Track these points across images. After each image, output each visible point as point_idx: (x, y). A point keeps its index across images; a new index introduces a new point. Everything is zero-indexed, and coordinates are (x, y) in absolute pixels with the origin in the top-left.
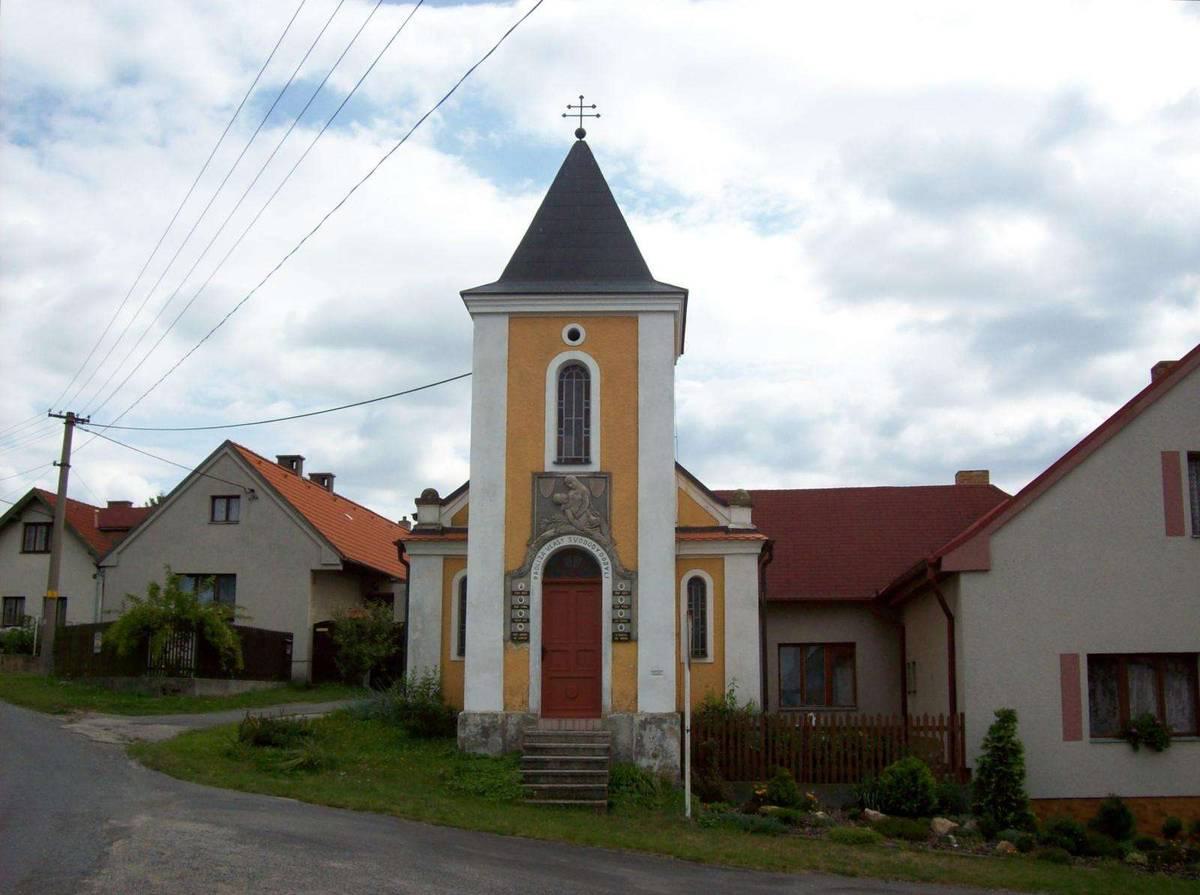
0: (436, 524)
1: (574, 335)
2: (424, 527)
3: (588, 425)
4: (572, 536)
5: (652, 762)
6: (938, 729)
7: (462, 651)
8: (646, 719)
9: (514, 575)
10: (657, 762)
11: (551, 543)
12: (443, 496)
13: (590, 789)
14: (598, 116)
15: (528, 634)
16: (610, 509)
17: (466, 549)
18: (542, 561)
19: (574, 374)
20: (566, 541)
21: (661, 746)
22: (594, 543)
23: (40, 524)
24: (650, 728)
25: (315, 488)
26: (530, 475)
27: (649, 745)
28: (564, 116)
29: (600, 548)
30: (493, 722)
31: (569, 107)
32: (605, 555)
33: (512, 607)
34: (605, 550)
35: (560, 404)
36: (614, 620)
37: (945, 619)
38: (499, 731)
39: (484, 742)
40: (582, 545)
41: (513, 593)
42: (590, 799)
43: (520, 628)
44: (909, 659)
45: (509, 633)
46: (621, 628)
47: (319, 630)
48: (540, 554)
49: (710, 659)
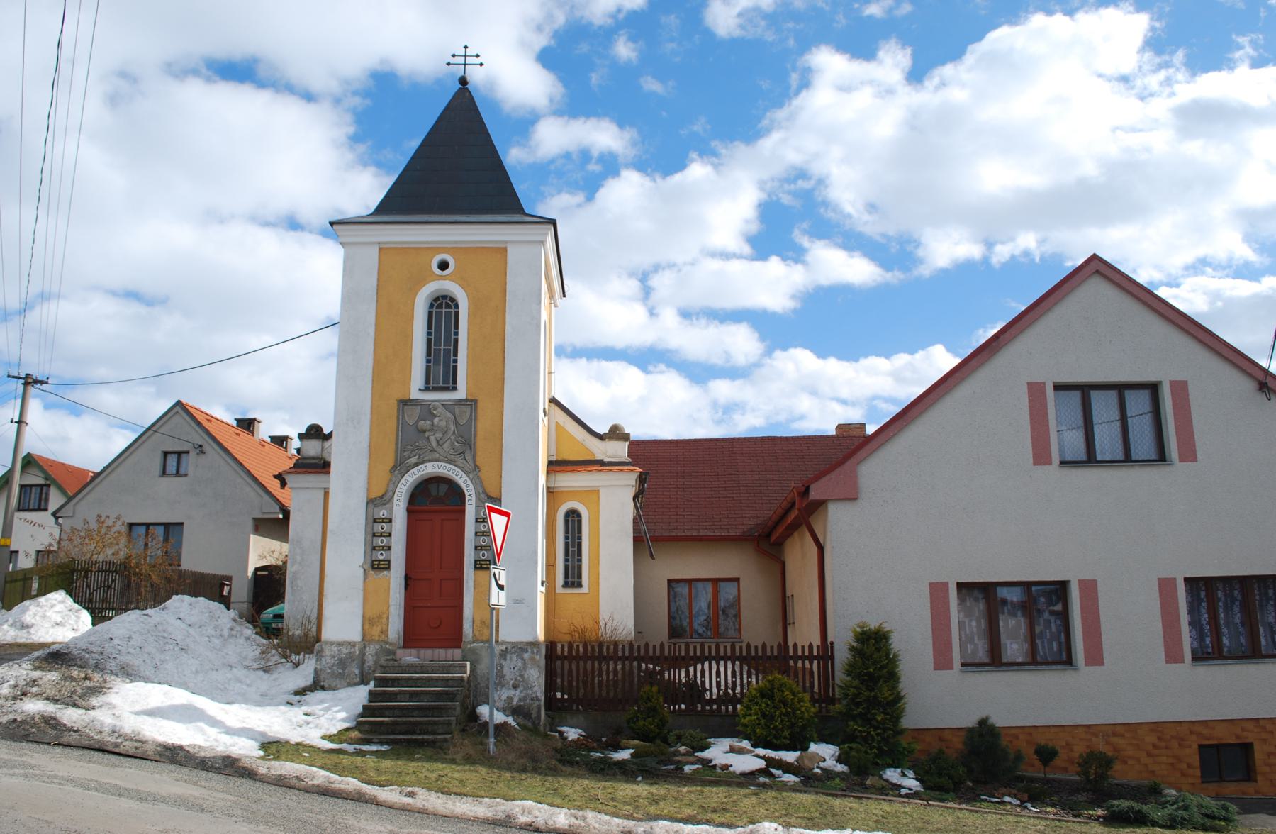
0: (318, 458)
2: (305, 461)
3: (456, 354)
5: (512, 692)
6: (807, 658)
10: (518, 693)
11: (415, 470)
13: (435, 723)
14: (481, 65)
15: (389, 561)
16: (475, 436)
18: (405, 488)
19: (443, 308)
20: (430, 469)
22: (457, 469)
23: (31, 486)
24: (511, 659)
26: (396, 402)
27: (509, 675)
29: (464, 475)
31: (454, 56)
32: (469, 482)
33: (374, 535)
34: (469, 477)
35: (429, 334)
37: (815, 549)
38: (356, 662)
39: (340, 674)
40: (446, 472)
41: (375, 521)
42: (434, 733)
43: (380, 556)
44: (788, 594)
45: (369, 562)
46: (483, 555)
47: (259, 573)
49: (585, 589)
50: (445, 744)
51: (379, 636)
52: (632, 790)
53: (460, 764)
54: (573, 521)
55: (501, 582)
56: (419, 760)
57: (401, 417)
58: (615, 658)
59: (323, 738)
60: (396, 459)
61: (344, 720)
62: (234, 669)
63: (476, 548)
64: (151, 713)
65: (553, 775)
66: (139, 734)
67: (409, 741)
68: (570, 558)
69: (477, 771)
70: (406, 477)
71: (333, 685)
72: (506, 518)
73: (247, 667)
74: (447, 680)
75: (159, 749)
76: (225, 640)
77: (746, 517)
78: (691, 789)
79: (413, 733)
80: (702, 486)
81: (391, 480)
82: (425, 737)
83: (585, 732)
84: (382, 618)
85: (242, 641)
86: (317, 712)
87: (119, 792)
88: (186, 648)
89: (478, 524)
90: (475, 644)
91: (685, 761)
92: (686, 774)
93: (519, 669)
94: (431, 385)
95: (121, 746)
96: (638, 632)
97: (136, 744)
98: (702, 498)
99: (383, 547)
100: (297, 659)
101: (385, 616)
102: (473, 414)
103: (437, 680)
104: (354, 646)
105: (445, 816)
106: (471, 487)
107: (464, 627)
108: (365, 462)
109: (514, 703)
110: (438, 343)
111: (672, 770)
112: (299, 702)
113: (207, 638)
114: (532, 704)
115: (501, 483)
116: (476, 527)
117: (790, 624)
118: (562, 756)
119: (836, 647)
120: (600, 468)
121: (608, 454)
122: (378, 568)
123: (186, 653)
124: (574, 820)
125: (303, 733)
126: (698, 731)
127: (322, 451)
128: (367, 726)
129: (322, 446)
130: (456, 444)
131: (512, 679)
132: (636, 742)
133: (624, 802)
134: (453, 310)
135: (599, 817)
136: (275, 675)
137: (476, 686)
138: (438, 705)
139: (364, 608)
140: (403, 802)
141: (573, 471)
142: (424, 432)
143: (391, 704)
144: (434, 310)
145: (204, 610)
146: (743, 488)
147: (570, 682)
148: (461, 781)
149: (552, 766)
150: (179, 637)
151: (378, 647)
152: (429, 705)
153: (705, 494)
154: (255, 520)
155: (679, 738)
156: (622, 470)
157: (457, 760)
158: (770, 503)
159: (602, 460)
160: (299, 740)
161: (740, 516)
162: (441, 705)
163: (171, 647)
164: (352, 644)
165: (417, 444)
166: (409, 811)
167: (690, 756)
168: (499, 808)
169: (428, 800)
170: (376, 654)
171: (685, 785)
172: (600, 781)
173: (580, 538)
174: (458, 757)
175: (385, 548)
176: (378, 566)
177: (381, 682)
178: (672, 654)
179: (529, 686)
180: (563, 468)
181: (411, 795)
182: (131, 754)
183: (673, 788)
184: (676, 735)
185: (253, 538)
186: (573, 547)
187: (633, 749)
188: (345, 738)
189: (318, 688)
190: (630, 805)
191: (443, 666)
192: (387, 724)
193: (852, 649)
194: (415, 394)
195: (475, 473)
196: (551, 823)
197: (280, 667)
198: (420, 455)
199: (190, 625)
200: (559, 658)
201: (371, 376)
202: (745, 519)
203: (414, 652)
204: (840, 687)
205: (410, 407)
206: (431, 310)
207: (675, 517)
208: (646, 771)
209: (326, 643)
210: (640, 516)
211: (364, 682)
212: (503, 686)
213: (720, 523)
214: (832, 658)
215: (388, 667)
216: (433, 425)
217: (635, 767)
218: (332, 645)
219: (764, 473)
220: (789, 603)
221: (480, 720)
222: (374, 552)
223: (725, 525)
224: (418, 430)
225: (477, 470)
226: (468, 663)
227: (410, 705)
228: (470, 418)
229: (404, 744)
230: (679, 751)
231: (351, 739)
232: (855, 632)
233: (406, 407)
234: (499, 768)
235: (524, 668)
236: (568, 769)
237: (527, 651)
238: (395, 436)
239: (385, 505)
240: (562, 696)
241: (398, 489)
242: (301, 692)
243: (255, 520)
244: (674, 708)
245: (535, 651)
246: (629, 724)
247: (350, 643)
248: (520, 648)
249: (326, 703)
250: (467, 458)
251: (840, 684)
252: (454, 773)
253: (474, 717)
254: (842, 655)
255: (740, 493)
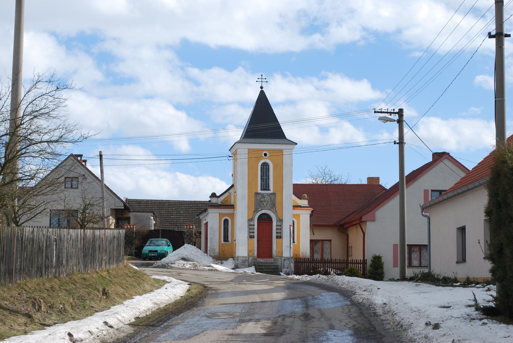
0: (216, 203)
1: (265, 155)
3: (261, 175)
5: (287, 269)
8: (285, 259)
9: (250, 220)
10: (288, 270)
12: (218, 195)
14: (267, 82)
15: (254, 236)
19: (265, 166)
20: (264, 211)
22: (271, 212)
24: (286, 261)
26: (254, 194)
27: (286, 265)
30: (245, 259)
31: (258, 79)
36: (277, 233)
41: (250, 225)
43: (252, 234)
44: (350, 245)
45: (249, 236)
46: (278, 235)
48: (257, 215)
49: (230, 243)
58: (304, 262)
60: (255, 209)
70: (258, 214)
71: (241, 267)
77: (334, 218)
98: (317, 210)
101: (253, 250)
108: (247, 209)
110: (264, 176)
117: (350, 256)
119: (367, 261)
121: (303, 204)
142: (262, 202)
146: (333, 206)
153: (318, 208)
158: (343, 213)
159: (301, 206)
161: (332, 217)
164: (246, 257)
176: (252, 237)
193: (372, 261)
194: (259, 191)
202: (334, 219)
204: (368, 270)
212: (284, 268)
213: (325, 220)
214: (366, 263)
219: (340, 200)
220: (350, 250)
224: (261, 201)
232: (373, 256)
247: (245, 257)
251: (368, 270)
254: (369, 262)
255: (331, 208)
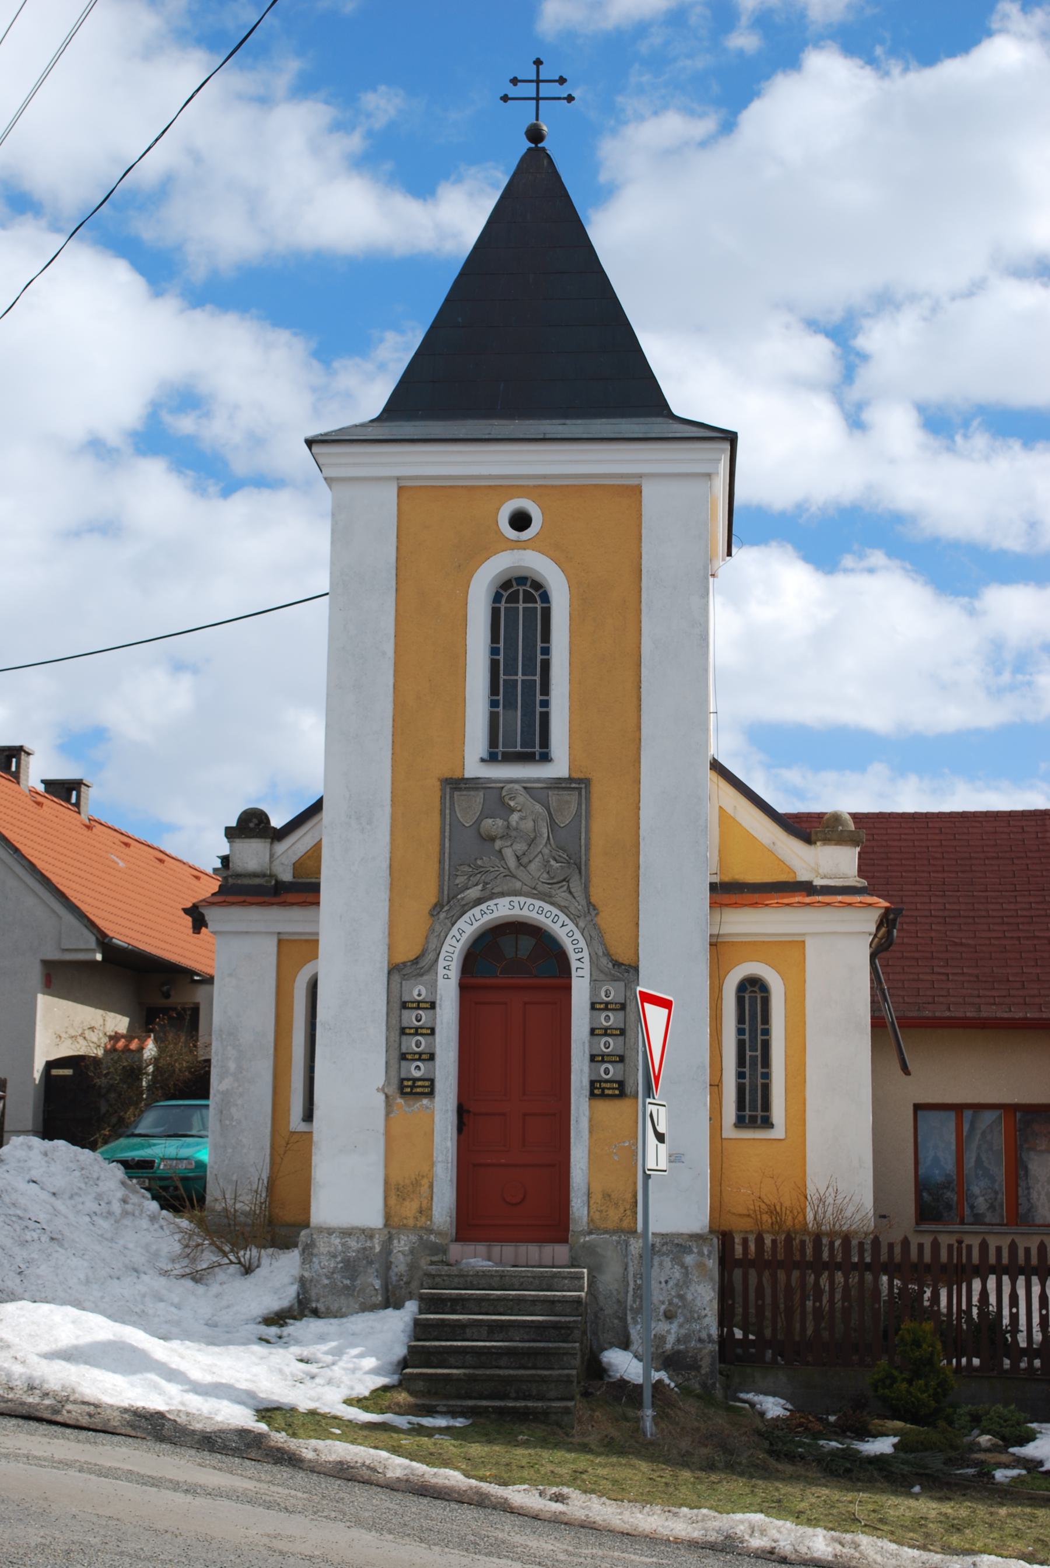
0: (264, 875)
1: (520, 521)
3: (546, 689)
4: (516, 899)
7: (308, 1116)
10: (674, 1327)
11: (476, 911)
12: (277, 821)
13: (544, 1380)
14: (570, 99)
15: (432, 1081)
17: (317, 922)
18: (459, 945)
21: (681, 1297)
22: (555, 911)
24: (661, 1264)
25: (53, 807)
27: (659, 1296)
28: (505, 98)
29: (567, 921)
31: (515, 81)
32: (578, 935)
33: (403, 1031)
34: (577, 925)
35: (494, 651)
38: (376, 1266)
39: (347, 1287)
40: (534, 915)
41: (404, 1005)
42: (541, 1398)
43: (416, 1070)
45: (395, 1082)
46: (607, 1072)
47: (55, 1072)
48: (454, 931)
49: (779, 1131)
50: (566, 1418)
51: (416, 1218)
52: (909, 1508)
53: (599, 1454)
54: (753, 1000)
55: (661, 1129)
56: (526, 1444)
57: (448, 811)
59: (349, 1402)
61: (376, 1372)
62: (144, 1277)
63: (593, 1058)
64: (69, 1355)
65: (764, 1478)
66: (74, 1391)
67: (501, 1412)
68: (747, 1070)
69: (633, 1467)
70: (461, 924)
71: (335, 1307)
72: (666, 1011)
73: (165, 1273)
74: (552, 1302)
75: (126, 1416)
76: (117, 1222)
78: (1013, 1510)
79: (504, 1397)
80: (984, 913)
81: (432, 930)
82: (530, 1404)
83: (792, 1404)
84: (421, 1185)
85: (145, 1223)
86: (320, 1355)
87: (155, 1482)
88: (60, 1237)
89: (596, 1013)
90: (593, 1236)
91: (993, 1461)
92: (1001, 1484)
93: (677, 1285)
94: (501, 749)
95: (64, 1412)
96: (881, 1216)
97: (86, 1408)
99: (420, 1054)
100: (247, 1256)
102: (584, 807)
103: (535, 1301)
104: (371, 1237)
105: (628, 1534)
106: (582, 944)
107: (573, 1204)
108: (384, 895)
109: (668, 1346)
111: (973, 1475)
112: (280, 1337)
113: (87, 1219)
114: (700, 1349)
115: (637, 936)
116: (592, 1019)
118: (771, 1444)
120: (808, 900)
122: (411, 1093)
123: (61, 1246)
124: (839, 1547)
125: (312, 1393)
126: (1013, 1407)
127: (271, 862)
128: (422, 1383)
129: (271, 850)
130: (553, 862)
131: (663, 1303)
132: (899, 1424)
133: (902, 1526)
134: (539, 605)
135: (880, 1544)
136: (215, 1288)
137: (596, 1316)
138: (543, 1348)
139: (387, 1166)
140: (553, 1509)
141: (754, 905)
142: (493, 839)
143: (459, 1344)
144: (503, 605)
145: (70, 1165)
147: (760, 1310)
148: (615, 1482)
149: (758, 1462)
150: (42, 1217)
151: (414, 1238)
152: (529, 1348)
154: (46, 964)
155: (976, 1420)
156: (849, 904)
157: (593, 1447)
160: (312, 1405)
162: (549, 1348)
163: (35, 1235)
164: (368, 1234)
165: (479, 862)
166: (566, 1524)
167: (1000, 1452)
168: (710, 1524)
169: (590, 1508)
170: (412, 1251)
171: (1002, 1504)
172: (848, 1490)
173: (766, 1032)
174: (592, 1440)
175: (424, 1057)
177: (430, 1304)
178: (955, 1261)
179: (696, 1315)
180: (735, 898)
181: (558, 1498)
182: (84, 1425)
183: (980, 1507)
184: (971, 1415)
185: (43, 1001)
186: (753, 1049)
187: (895, 1436)
188: (387, 1403)
189: (307, 1312)
190: (913, 1531)
191: (541, 1277)
192: (458, 1379)
194: (474, 768)
195: (588, 918)
196: (803, 1550)
197: (221, 1275)
198: (486, 884)
199: (54, 1194)
200: (739, 1263)
201: (391, 734)
203: (481, 1248)
205: (464, 793)
206: (497, 605)
207: (929, 977)
208: (926, 1475)
209: (320, 1230)
210: (882, 991)
211: (391, 1301)
215: (440, 1276)
216: (508, 827)
217: (906, 1469)
218: (330, 1234)
221: (610, 1376)
222: (403, 1063)
223: (1034, 996)
225: (593, 913)
226: (585, 1270)
227: (493, 1347)
228: (578, 814)
229: (493, 1416)
230: (979, 1443)
231: (398, 1404)
233: (456, 794)
234: (667, 1461)
235: (686, 1281)
236: (789, 1469)
237: (691, 1252)
238: (437, 849)
239: (422, 975)
240: (746, 1335)
241: (446, 947)
242: (278, 1319)
243: (46, 964)
244: (959, 1362)
245: (706, 1253)
246: (876, 1391)
247: (363, 1231)
248: (678, 1245)
249: (333, 1341)
250: (573, 890)
252: (602, 1467)
253: (596, 1370)
